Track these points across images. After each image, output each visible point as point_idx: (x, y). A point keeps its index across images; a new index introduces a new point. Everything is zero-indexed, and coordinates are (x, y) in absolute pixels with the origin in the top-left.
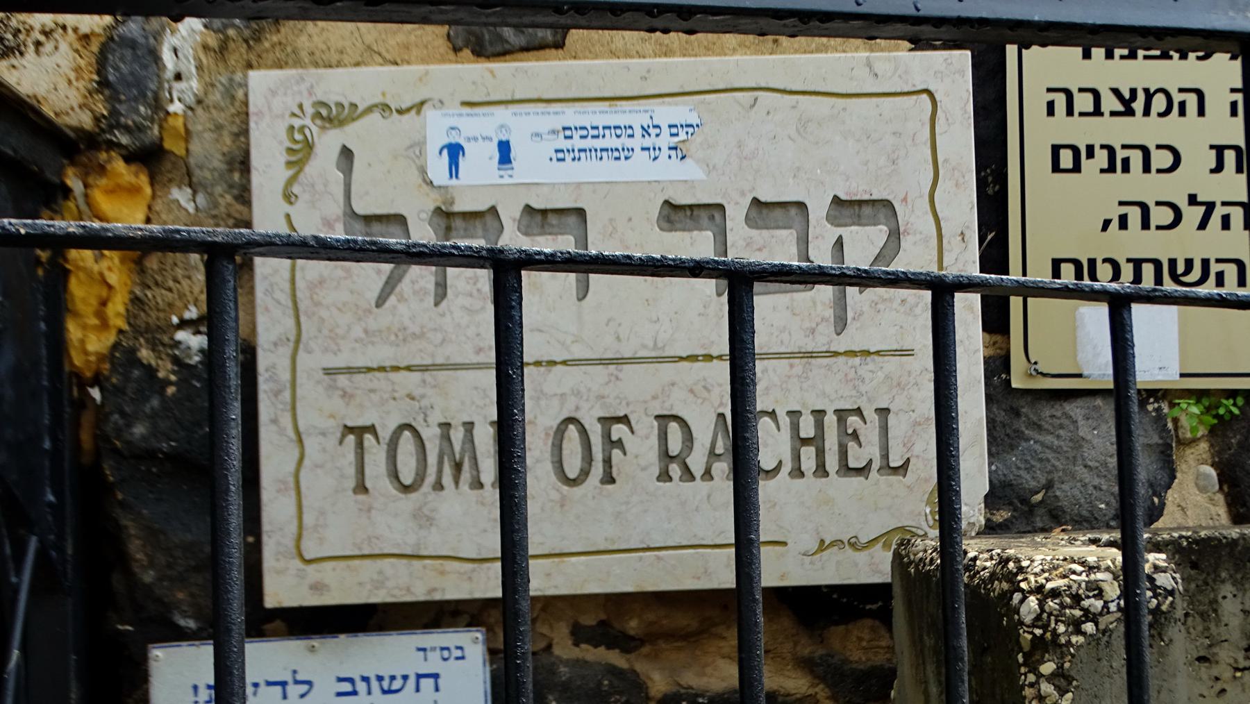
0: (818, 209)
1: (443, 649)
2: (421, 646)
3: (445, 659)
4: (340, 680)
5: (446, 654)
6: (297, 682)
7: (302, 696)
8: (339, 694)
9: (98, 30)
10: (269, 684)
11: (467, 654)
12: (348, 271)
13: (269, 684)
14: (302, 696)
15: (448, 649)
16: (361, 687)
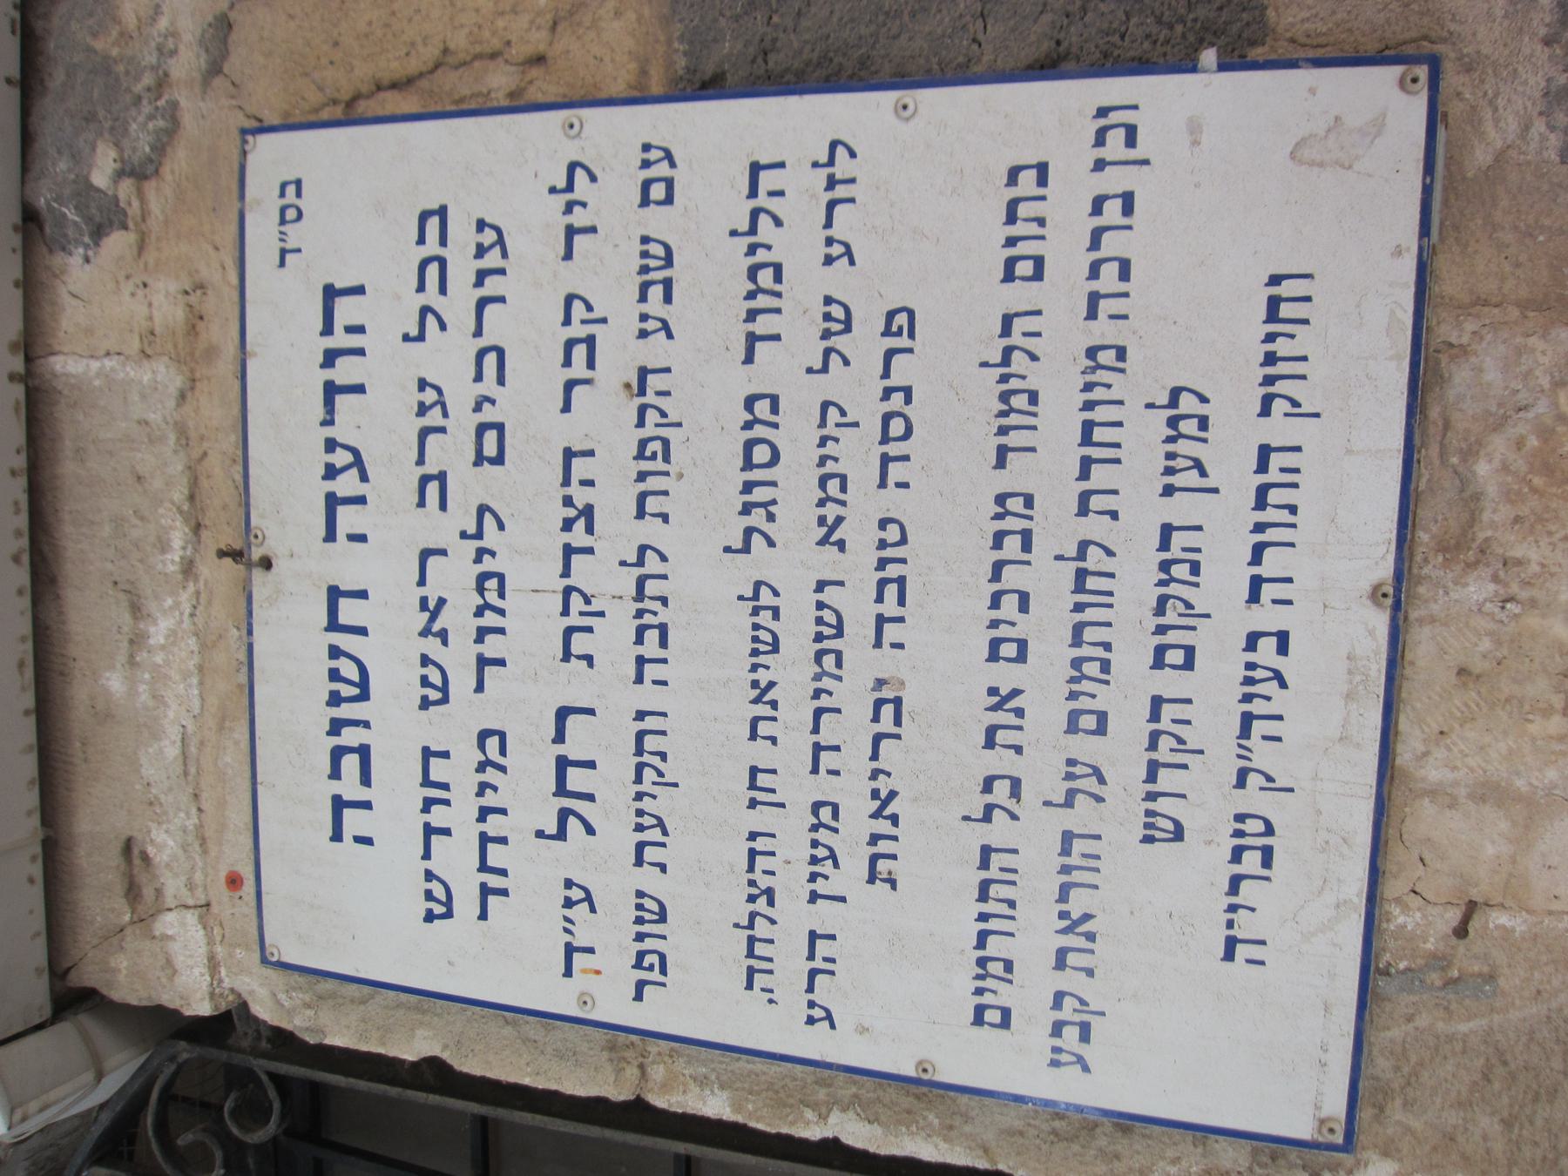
0: (984, 875)
1: (283, 221)
2: (1220, 951)
3: (300, 215)
4: (421, 503)
5: (291, 214)
6: (831, 162)
7: (853, 155)
8: (443, 506)
9: (181, 980)
10: (427, 855)
11: (292, 178)
12: (1398, 252)
13: (427, 855)
14: (853, 155)
15: (283, 210)
16: (892, 571)
